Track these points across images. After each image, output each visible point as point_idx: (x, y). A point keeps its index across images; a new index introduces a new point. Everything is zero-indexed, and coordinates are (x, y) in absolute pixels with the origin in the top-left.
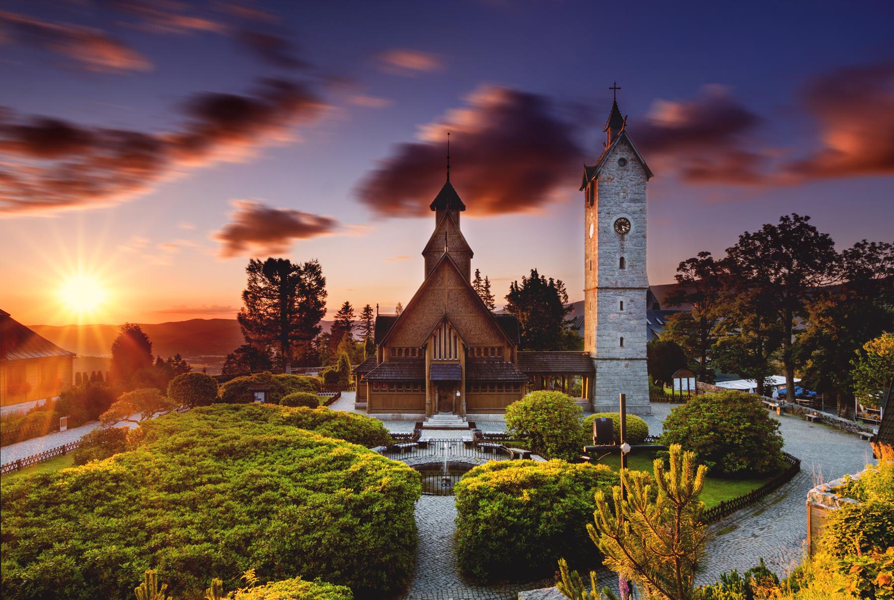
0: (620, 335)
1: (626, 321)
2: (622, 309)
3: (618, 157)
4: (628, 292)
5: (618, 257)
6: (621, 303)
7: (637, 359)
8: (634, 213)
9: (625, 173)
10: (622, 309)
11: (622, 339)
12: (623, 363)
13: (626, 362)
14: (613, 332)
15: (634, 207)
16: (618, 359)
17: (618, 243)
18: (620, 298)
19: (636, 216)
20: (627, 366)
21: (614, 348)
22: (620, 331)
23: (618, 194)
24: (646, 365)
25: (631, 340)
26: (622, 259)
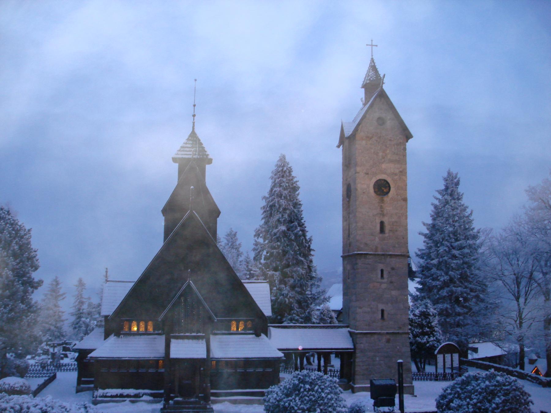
0: (381, 306)
4: (388, 259)
5: (378, 221)
6: (382, 271)
7: (398, 333)
11: (383, 311)
12: (384, 339)
13: (388, 337)
20: (388, 341)
26: (382, 224)
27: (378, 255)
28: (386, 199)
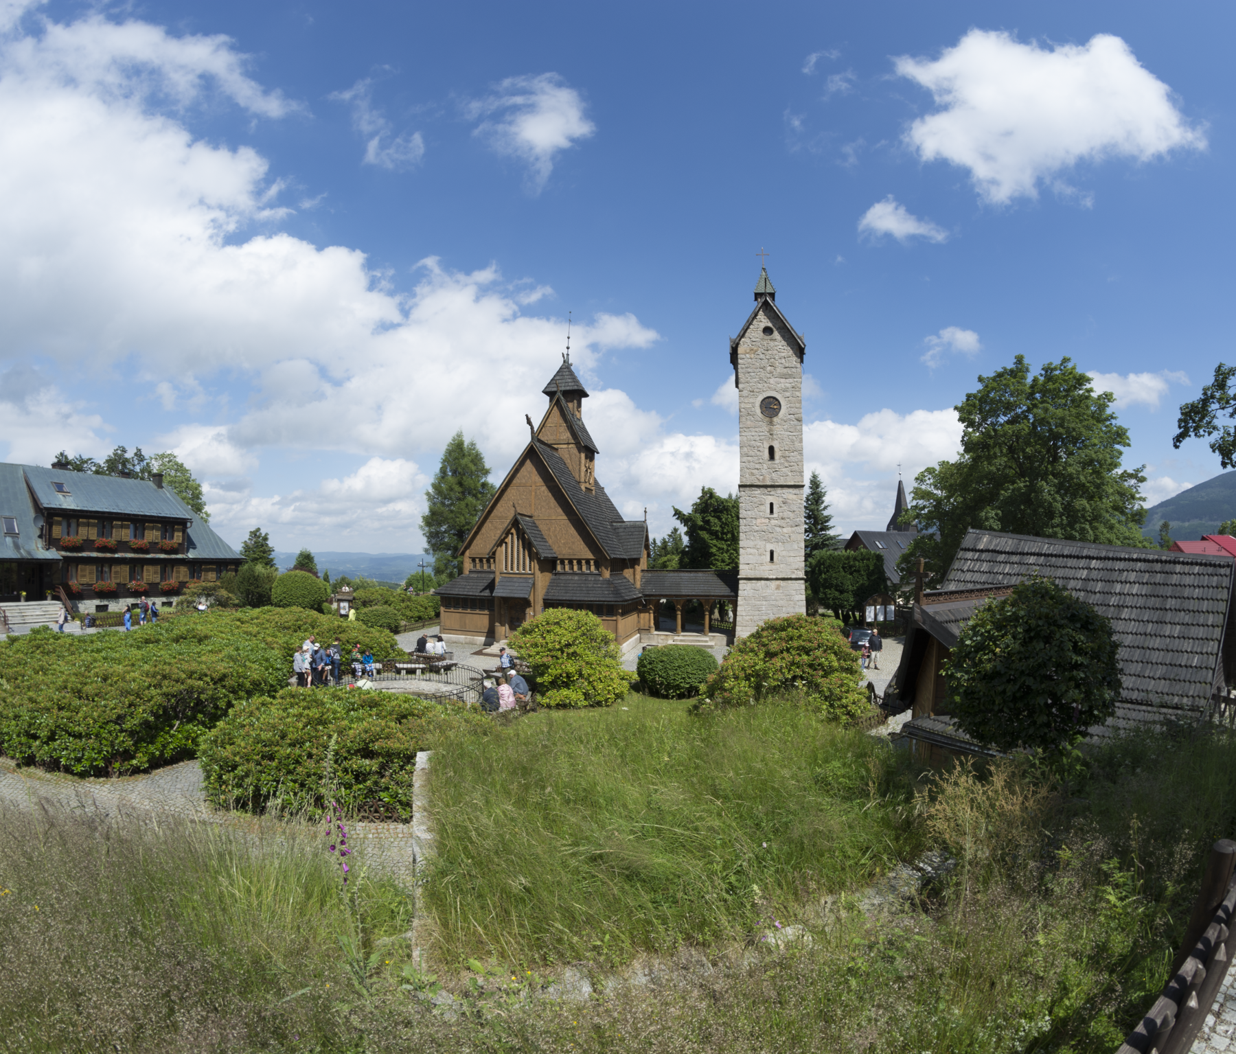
0: (770, 547)
1: (778, 529)
2: (772, 512)
3: (763, 325)
4: (779, 491)
5: (767, 446)
6: (772, 505)
7: (791, 579)
8: (785, 390)
9: (772, 344)
10: (772, 512)
11: (772, 553)
14: (760, 543)
15: (784, 383)
16: (767, 579)
17: (765, 428)
18: (770, 499)
19: (788, 394)
20: (778, 588)
21: (762, 564)
22: (768, 540)
23: (764, 368)
24: (803, 587)
25: (784, 553)
26: (771, 449)
27: (766, 487)
28: (775, 419)
